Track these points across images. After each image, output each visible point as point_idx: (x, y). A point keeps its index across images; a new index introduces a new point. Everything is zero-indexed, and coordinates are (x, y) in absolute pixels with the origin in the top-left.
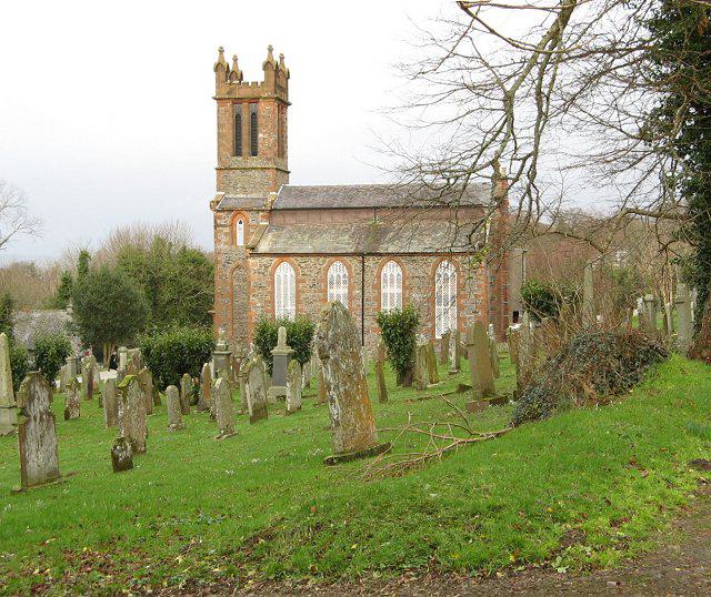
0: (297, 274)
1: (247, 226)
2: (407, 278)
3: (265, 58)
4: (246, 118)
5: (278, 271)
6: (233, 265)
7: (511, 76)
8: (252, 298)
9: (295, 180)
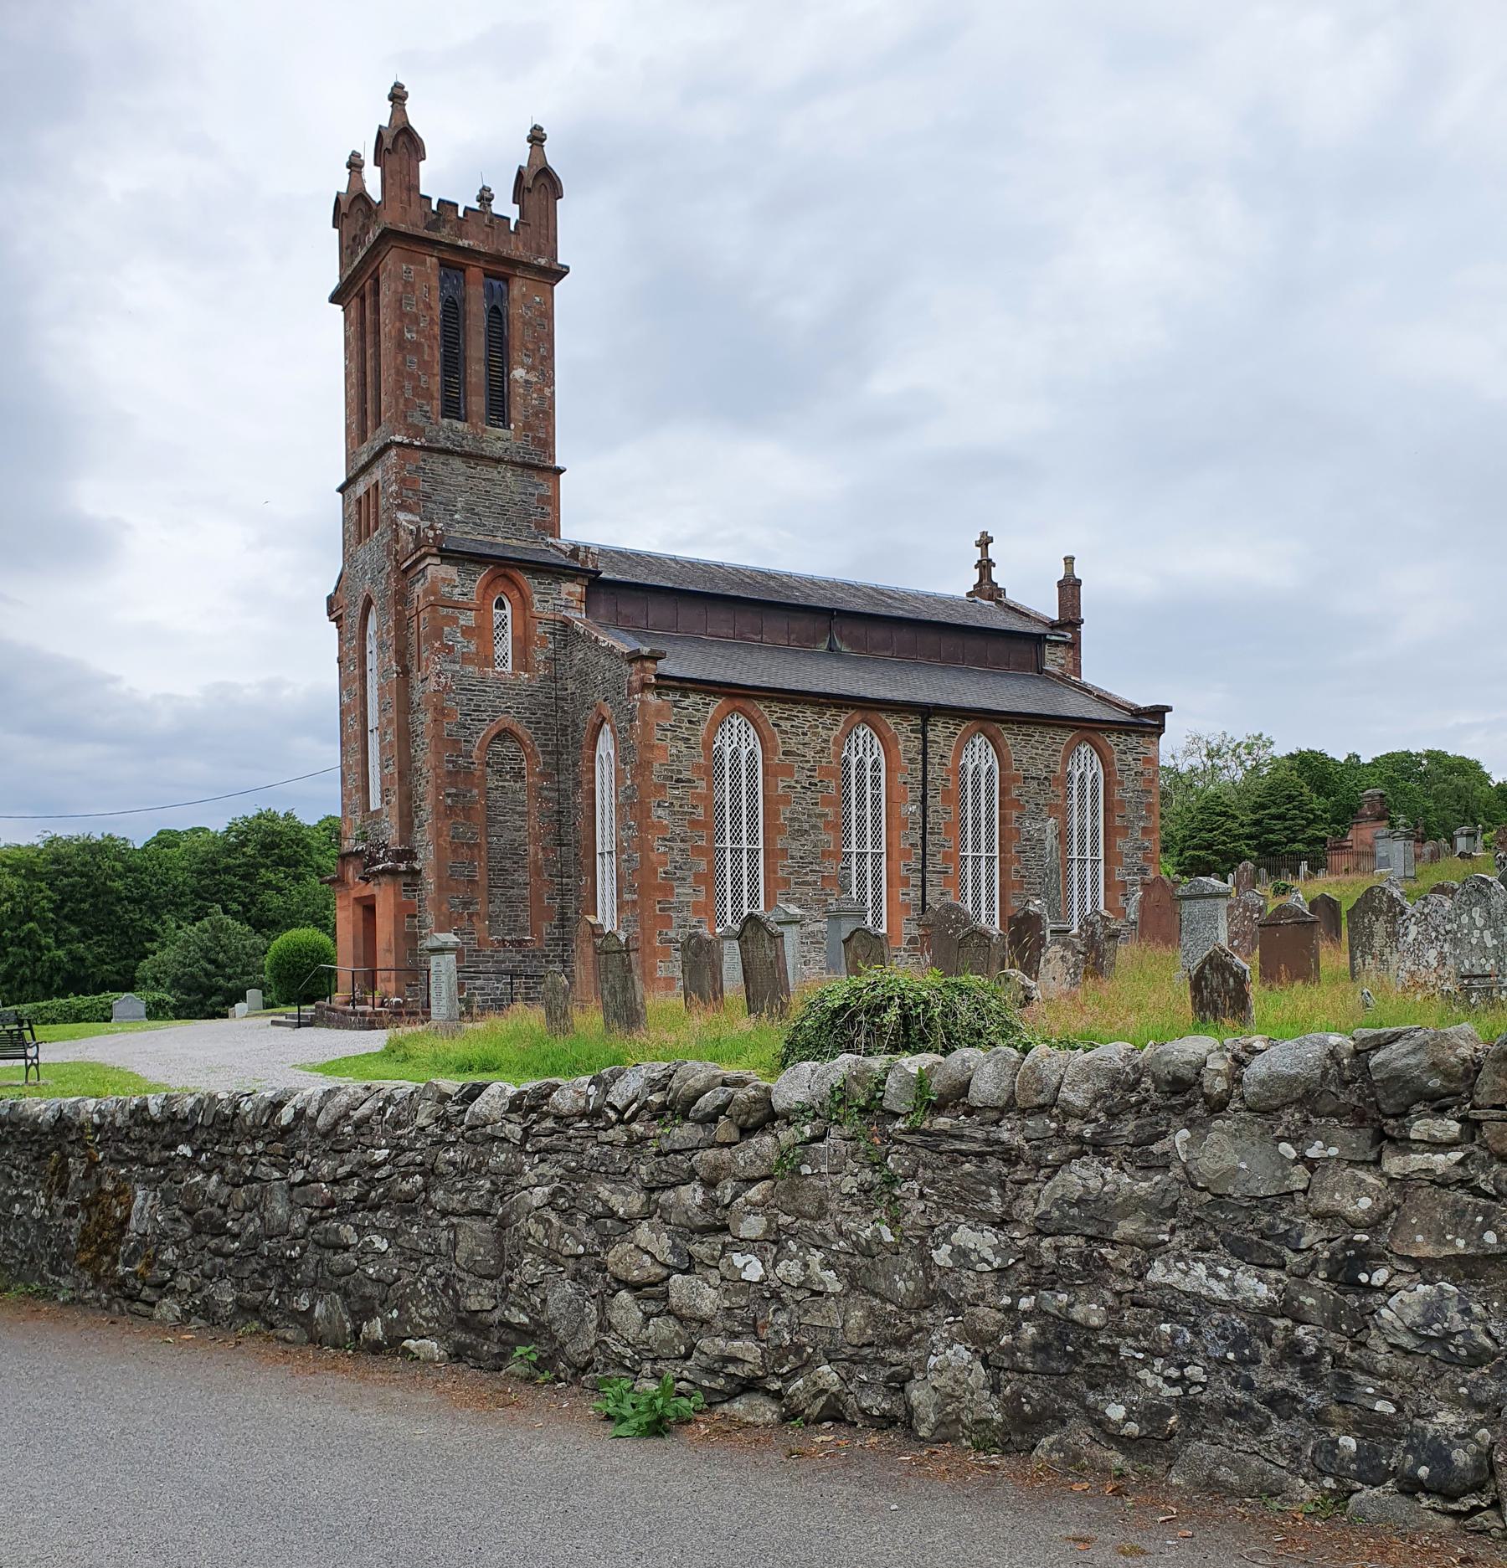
2: (1015, 779)
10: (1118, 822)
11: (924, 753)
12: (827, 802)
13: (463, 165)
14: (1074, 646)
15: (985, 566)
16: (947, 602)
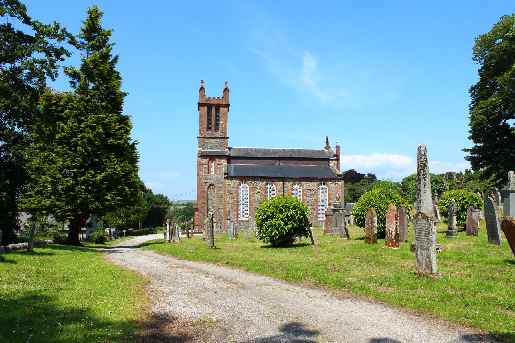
2: (305, 190)
3: (197, 99)
6: (208, 184)
7: (204, 272)
8: (226, 198)
11: (283, 186)
12: (262, 196)
13: (214, 92)
15: (327, 143)
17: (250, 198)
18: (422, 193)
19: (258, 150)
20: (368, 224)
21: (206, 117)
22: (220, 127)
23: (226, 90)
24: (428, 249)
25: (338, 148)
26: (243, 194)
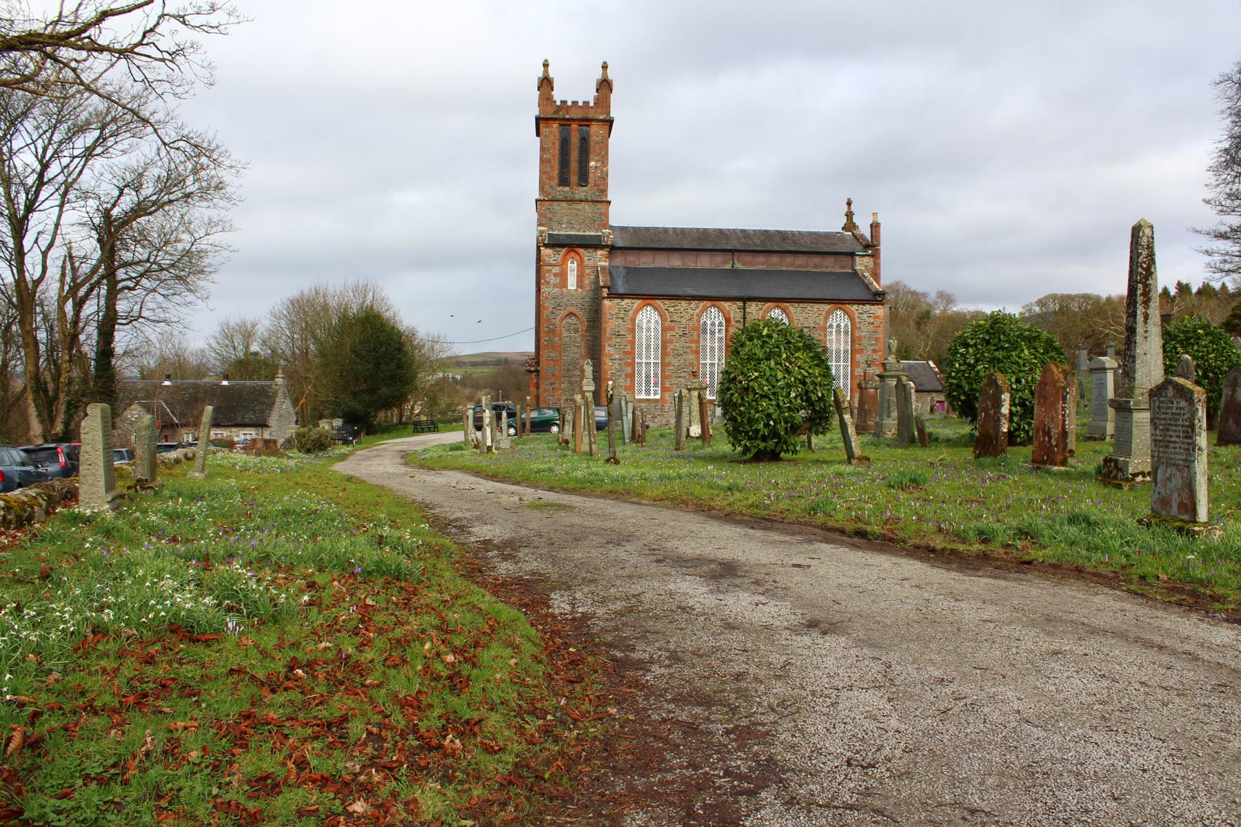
0: (663, 319)
1: (581, 266)
4: (575, 140)
5: (639, 317)
9: (615, 220)
10: (857, 347)
13: (575, 89)
14: (875, 256)
15: (849, 215)
16: (828, 236)
17: (664, 347)
18: (1139, 339)
19: (683, 231)
20: (986, 410)
21: (557, 152)
22: (591, 175)
23: (605, 86)
24: (1188, 467)
25: (875, 227)
26: (648, 339)
